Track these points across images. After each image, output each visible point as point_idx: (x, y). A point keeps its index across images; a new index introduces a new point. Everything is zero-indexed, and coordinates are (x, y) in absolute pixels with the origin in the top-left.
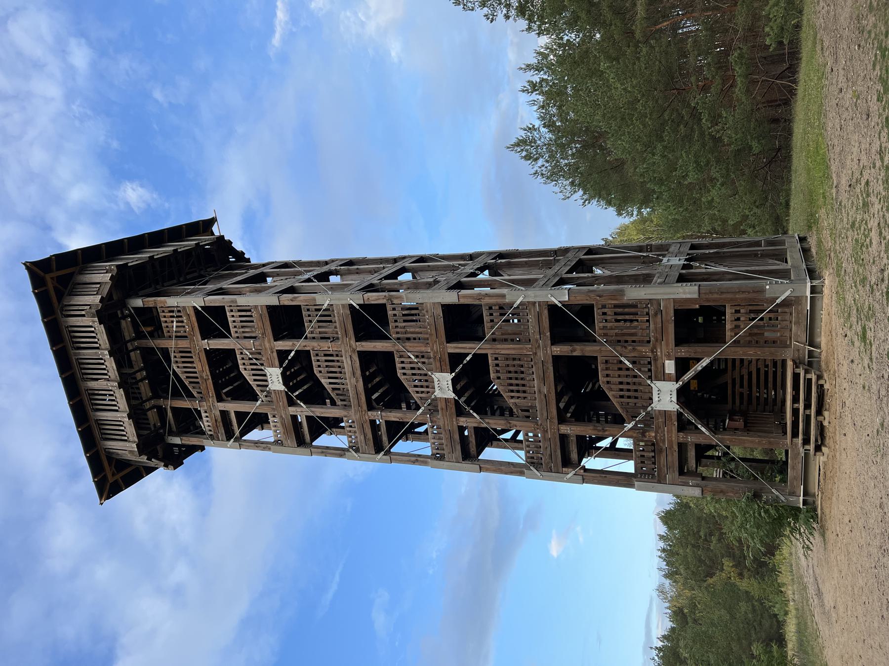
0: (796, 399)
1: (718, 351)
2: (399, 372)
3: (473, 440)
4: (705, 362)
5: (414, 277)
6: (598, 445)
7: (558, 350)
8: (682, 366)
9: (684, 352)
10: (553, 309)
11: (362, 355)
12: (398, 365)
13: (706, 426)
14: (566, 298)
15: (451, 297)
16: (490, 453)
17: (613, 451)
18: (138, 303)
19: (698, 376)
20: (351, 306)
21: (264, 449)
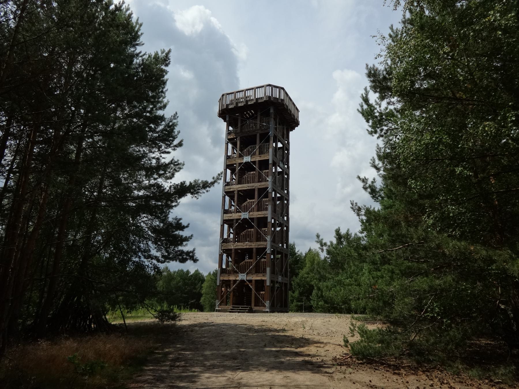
0: (241, 307)
1: (253, 290)
4: (251, 287)
6: (230, 257)
7: (254, 250)
8: (254, 162)
9: (257, 163)
10: (266, 248)
11: (254, 189)
14: (268, 252)
16: (227, 198)
17: (227, 262)
18: (272, 111)
19: (248, 285)
20: (268, 188)
21: (225, 153)
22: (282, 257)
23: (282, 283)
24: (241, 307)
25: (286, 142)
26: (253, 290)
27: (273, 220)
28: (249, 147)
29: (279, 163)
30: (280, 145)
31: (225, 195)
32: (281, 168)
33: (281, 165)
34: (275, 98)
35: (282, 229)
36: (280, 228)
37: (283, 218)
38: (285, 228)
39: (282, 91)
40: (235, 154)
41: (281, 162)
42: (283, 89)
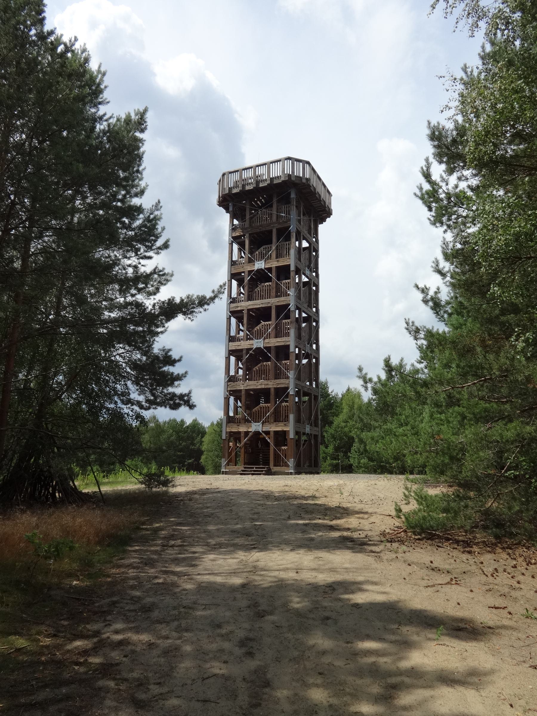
0: (256, 468)
1: (272, 444)
2: (264, 247)
3: (241, 240)
4: (269, 441)
5: (305, 249)
8: (270, 270)
9: (272, 434)
10: (287, 388)
12: (267, 246)
13: (248, 440)
14: (291, 393)
15: (292, 268)
17: (236, 408)
18: (293, 196)
19: (264, 438)
20: (289, 305)
22: (310, 400)
23: (311, 434)
24: (256, 468)
25: (314, 239)
26: (272, 444)
27: (297, 349)
28: (262, 248)
29: (305, 270)
30: (305, 244)
31: (230, 317)
32: (307, 277)
33: (308, 272)
34: (298, 177)
35: (310, 362)
36: (306, 360)
37: (311, 346)
38: (314, 360)
39: (307, 166)
40: (243, 258)
41: (307, 269)
42: (308, 163)
